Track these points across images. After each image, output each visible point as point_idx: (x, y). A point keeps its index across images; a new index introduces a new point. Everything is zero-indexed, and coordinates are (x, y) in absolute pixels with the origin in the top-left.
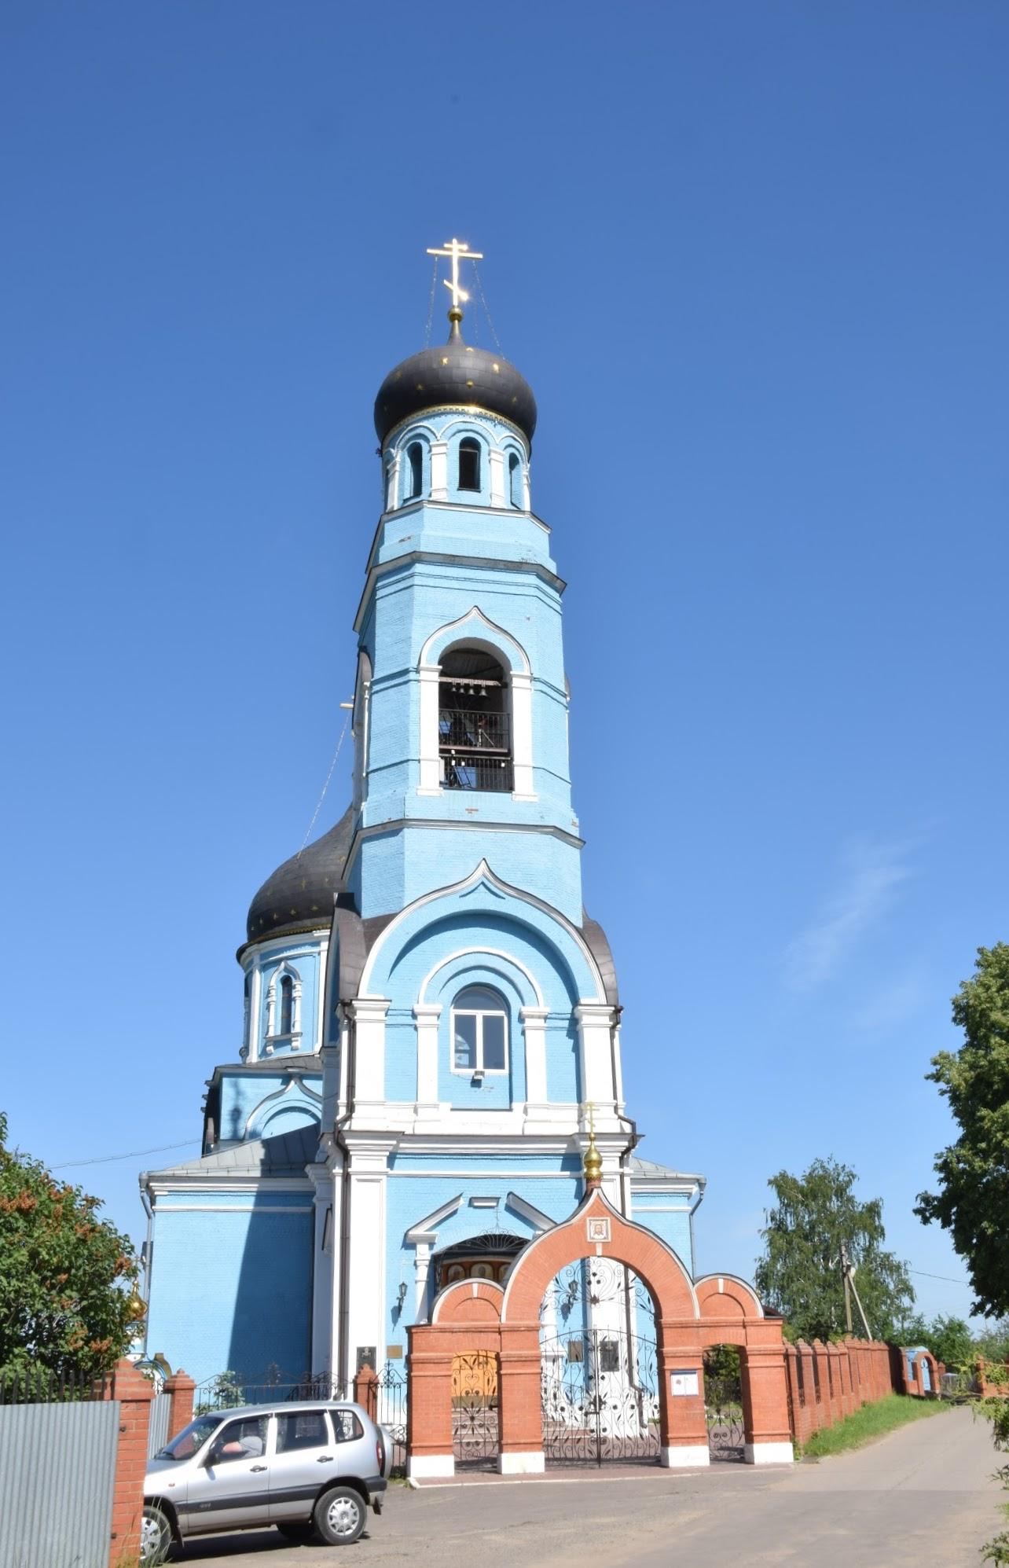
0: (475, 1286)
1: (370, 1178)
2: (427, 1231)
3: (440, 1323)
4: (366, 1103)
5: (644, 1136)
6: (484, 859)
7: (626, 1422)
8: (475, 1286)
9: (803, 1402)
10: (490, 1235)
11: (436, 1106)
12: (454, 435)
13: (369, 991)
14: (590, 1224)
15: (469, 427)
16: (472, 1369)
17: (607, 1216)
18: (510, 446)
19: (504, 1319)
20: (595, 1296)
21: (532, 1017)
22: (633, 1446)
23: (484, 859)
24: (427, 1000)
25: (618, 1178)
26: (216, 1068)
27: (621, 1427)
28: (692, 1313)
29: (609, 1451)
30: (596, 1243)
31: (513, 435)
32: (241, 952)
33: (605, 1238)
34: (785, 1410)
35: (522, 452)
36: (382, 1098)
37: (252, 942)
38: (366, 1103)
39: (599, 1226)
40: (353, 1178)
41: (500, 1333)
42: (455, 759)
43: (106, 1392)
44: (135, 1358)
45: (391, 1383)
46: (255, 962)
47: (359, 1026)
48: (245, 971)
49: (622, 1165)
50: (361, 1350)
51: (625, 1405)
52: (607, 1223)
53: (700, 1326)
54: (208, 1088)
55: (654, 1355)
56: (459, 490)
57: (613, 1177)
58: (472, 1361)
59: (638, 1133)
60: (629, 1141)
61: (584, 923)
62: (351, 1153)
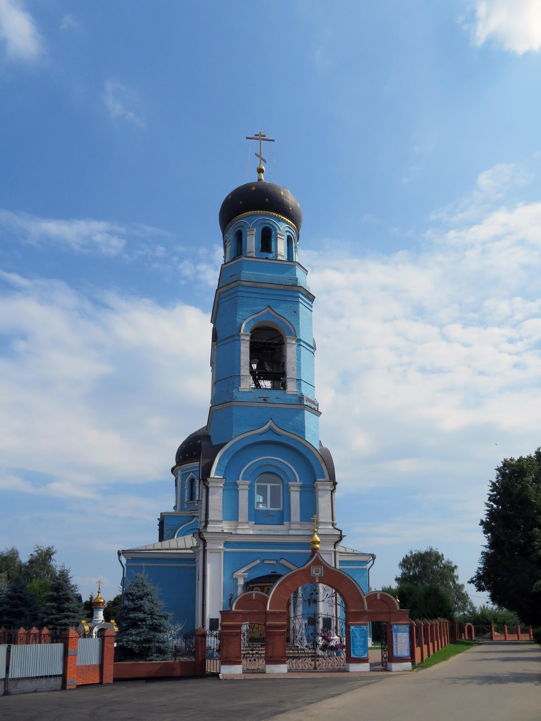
0: (254, 595)
2: (242, 573)
3: (235, 610)
5: (346, 536)
6: (271, 418)
8: (254, 595)
9: (265, 136)
16: (252, 629)
19: (268, 609)
20: (315, 599)
23: (271, 418)
24: (243, 479)
26: (161, 513)
28: (364, 607)
29: (320, 664)
30: (315, 577)
31: (289, 226)
32: (173, 470)
33: (320, 575)
36: (221, 519)
38: (213, 521)
40: (208, 552)
43: (220, 622)
45: (213, 635)
46: (179, 473)
49: (335, 548)
52: (321, 569)
55: (344, 625)
56: (260, 252)
57: (331, 552)
58: (253, 626)
59: (343, 535)
60: (339, 538)
61: (304, 414)
62: (207, 541)
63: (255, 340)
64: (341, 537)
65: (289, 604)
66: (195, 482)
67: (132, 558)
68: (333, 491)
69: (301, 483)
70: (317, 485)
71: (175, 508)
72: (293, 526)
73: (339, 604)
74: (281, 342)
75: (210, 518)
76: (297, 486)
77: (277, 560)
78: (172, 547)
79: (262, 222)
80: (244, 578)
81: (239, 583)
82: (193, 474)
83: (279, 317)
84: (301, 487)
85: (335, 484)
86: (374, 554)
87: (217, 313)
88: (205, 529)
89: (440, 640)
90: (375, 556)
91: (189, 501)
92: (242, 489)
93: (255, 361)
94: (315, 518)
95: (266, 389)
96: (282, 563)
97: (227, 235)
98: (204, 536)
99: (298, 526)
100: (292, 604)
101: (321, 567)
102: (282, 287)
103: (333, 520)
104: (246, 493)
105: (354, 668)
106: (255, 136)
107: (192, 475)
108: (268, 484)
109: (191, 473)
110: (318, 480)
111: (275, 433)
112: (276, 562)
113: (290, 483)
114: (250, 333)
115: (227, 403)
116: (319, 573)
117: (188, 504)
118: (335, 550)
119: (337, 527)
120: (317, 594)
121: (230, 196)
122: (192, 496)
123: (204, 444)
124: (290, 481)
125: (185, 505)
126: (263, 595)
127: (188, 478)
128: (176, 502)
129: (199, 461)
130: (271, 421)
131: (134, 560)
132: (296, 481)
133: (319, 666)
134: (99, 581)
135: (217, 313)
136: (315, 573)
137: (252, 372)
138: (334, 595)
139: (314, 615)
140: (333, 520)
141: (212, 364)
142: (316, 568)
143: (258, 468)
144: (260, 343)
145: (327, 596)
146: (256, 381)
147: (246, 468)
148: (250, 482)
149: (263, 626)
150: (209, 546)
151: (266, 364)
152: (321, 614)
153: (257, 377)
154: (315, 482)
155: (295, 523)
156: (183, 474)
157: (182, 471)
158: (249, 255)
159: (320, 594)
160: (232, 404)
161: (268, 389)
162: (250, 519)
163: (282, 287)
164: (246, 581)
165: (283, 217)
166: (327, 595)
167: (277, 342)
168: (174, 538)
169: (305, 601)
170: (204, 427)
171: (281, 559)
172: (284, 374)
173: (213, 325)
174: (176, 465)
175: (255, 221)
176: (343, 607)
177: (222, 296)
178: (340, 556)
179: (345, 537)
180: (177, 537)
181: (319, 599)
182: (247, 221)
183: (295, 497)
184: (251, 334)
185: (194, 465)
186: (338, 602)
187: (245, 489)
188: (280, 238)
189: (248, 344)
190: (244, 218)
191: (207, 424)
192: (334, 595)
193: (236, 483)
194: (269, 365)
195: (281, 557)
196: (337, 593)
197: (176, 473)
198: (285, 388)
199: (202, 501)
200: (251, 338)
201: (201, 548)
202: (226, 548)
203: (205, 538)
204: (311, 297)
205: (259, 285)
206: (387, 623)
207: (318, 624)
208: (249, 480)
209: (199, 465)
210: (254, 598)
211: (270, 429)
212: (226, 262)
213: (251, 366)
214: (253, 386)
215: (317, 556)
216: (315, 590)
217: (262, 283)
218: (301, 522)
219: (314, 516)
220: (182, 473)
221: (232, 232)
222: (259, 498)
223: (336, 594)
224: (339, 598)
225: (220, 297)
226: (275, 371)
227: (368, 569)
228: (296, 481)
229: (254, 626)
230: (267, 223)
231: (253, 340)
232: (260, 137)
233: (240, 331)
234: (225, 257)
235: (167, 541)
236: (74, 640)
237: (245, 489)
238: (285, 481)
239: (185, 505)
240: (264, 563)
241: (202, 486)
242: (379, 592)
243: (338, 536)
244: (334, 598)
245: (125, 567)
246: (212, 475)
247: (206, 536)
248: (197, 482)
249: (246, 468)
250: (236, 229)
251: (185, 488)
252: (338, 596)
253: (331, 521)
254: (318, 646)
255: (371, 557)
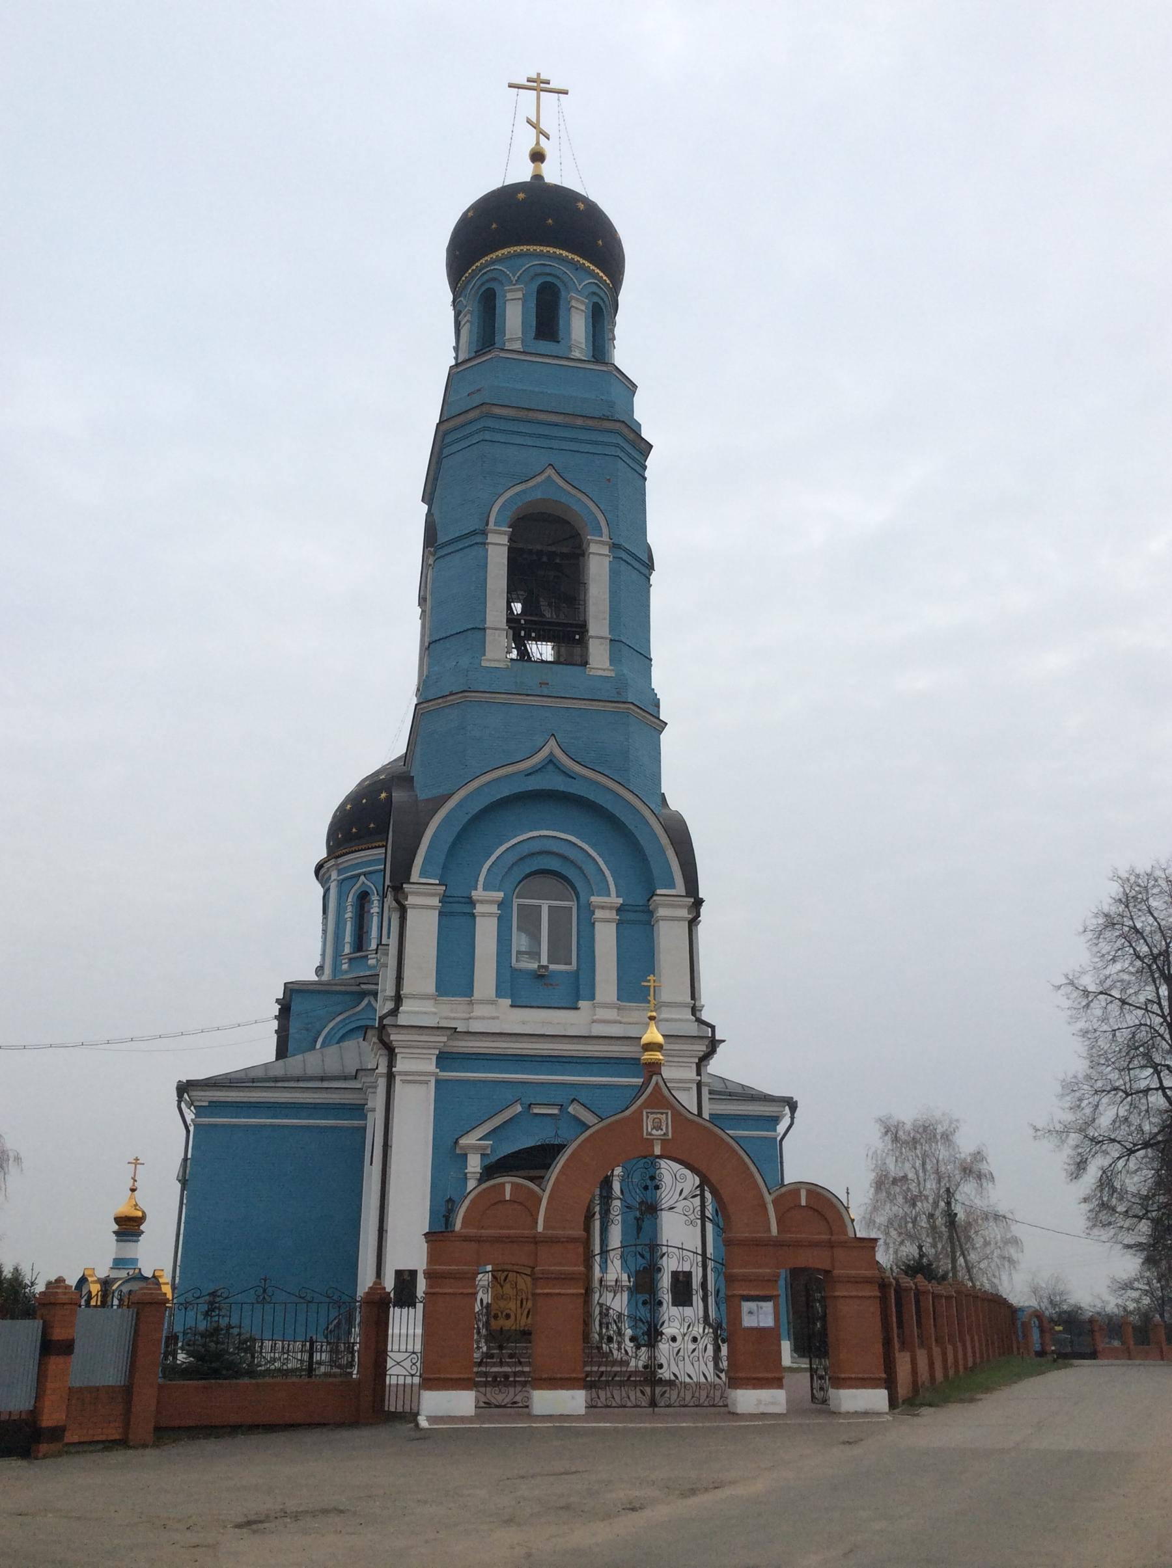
0: (508, 1188)
1: (415, 1079)
2: (479, 1140)
4: (413, 997)
5: (724, 1041)
6: (553, 735)
7: (686, 1357)
8: (508, 1188)
10: (548, 1145)
11: (492, 1002)
12: (532, 279)
13: (423, 874)
14: (648, 1117)
15: (547, 270)
16: (502, 1286)
17: (668, 1109)
18: (594, 293)
19: (540, 1229)
20: (652, 1204)
21: (603, 908)
22: (709, 1388)
24: (486, 888)
25: (695, 1087)
27: (681, 1364)
28: (769, 1230)
31: (596, 281)
32: (319, 868)
33: (665, 1134)
34: (878, 1348)
35: (607, 302)
37: (330, 858)
38: (413, 997)
39: (656, 1120)
40: (398, 1079)
41: (536, 1243)
42: (524, 629)
44: (128, 1274)
46: (333, 878)
47: (410, 914)
48: (323, 887)
50: (399, 1273)
51: (686, 1338)
52: (667, 1119)
53: (778, 1244)
54: (279, 1007)
58: (503, 1278)
59: (717, 1038)
62: (397, 1050)
63: (520, 545)
64: (713, 1044)
65: (589, 1217)
66: (369, 901)
67: (210, 1102)
68: (693, 922)
69: (620, 901)
70: (658, 906)
71: (320, 970)
72: (602, 1014)
73: (711, 1217)
74: (577, 551)
75: (405, 990)
76: (611, 908)
77: (562, 1105)
78: (310, 1071)
79: (539, 270)
80: (481, 1154)
81: (469, 1169)
82: (366, 881)
83: (574, 492)
84: (619, 910)
85: (699, 903)
86: (792, 1098)
87: (436, 479)
88: (394, 1018)
89: (959, 1344)
90: (796, 1102)
91: (354, 953)
92: (483, 915)
93: (518, 595)
94: (652, 981)
95: (542, 661)
96: (573, 1113)
97: (462, 299)
98: (389, 1036)
99: (612, 1014)
100: (597, 1216)
101: (667, 1114)
102: (579, 422)
103: (693, 997)
104: (494, 922)
105: (748, 1400)
106: (528, 81)
107: (363, 882)
108: (543, 901)
109: (362, 878)
110: (659, 892)
111: (564, 772)
112: (560, 1109)
113: (593, 899)
114: (509, 527)
115: (453, 694)
116: (662, 1130)
117: (350, 959)
118: (699, 1078)
119: (705, 1016)
120: (657, 1187)
121: (472, 212)
122: (360, 942)
123: (398, 796)
124: (593, 895)
125: (343, 961)
126: (528, 1188)
127: (353, 891)
128: (323, 955)
129: (383, 846)
130: (552, 742)
131: (216, 1107)
132: (609, 895)
133: (662, 1396)
134: (137, 1159)
135: (436, 479)
136: (652, 1129)
137: (512, 620)
138: (698, 1192)
139: (650, 1248)
140: (693, 997)
141: (422, 600)
142: (655, 1116)
143: (522, 859)
144: (530, 552)
145: (680, 1194)
146: (520, 643)
147: (493, 858)
148: (501, 894)
149: (528, 1279)
150: (401, 1066)
151: (543, 603)
152: (667, 1246)
153: (523, 633)
154: (651, 897)
155: (606, 1006)
156: (343, 880)
157: (340, 872)
158: (508, 346)
159: (663, 1189)
160: (467, 697)
161: (547, 662)
162: (499, 993)
163: (579, 422)
164: (487, 1162)
165: (584, 261)
166: (682, 1191)
167: (565, 550)
168: (314, 1048)
169: (627, 1207)
170: (395, 760)
171: (572, 1101)
172: (583, 628)
173: (427, 507)
174: (326, 856)
175: (524, 269)
176: (719, 1227)
177: (448, 440)
178: (711, 1101)
179: (723, 1044)
180: (323, 1046)
181: (663, 1202)
182: (506, 268)
183: (606, 938)
184: (511, 530)
185: (372, 857)
186: (708, 1214)
187: (490, 915)
188: (577, 308)
189: (504, 551)
190: (493, 262)
191: (405, 751)
192: (698, 1192)
193: (470, 898)
194: (550, 605)
195: (572, 1097)
196: (706, 1188)
197: (326, 877)
198: (585, 663)
199: (388, 945)
200: (510, 540)
201: (382, 1069)
202: (440, 1071)
203: (392, 1041)
204: (643, 445)
205: (531, 415)
206: (827, 1273)
207: (659, 1275)
208: (499, 890)
209: (383, 856)
210: (508, 1198)
211: (551, 760)
212: (459, 361)
213: (509, 608)
214: (514, 654)
215: (657, 1083)
216: (653, 1178)
217: (538, 412)
218: (619, 1002)
219: (649, 978)
220: (341, 877)
221: (473, 292)
222: (520, 941)
223: (703, 1191)
224: (710, 1201)
225: (445, 442)
226: (563, 619)
227: (779, 1139)
228: (609, 895)
229: (507, 1276)
230: (550, 274)
231: (514, 545)
232: (538, 85)
233: (487, 525)
234: (456, 349)
235: (299, 1057)
236: (68, 1311)
237: (490, 915)
238: (582, 895)
239: (343, 961)
240: (531, 1112)
241: (389, 901)
242: (803, 1186)
243: (707, 1042)
244: (697, 1200)
245: (192, 1129)
246: (415, 877)
247: (395, 1037)
248: (375, 898)
249: (493, 858)
250: (482, 284)
251: (346, 916)
252: (708, 1195)
253: (688, 999)
254: (659, 1338)
255: (784, 1107)
